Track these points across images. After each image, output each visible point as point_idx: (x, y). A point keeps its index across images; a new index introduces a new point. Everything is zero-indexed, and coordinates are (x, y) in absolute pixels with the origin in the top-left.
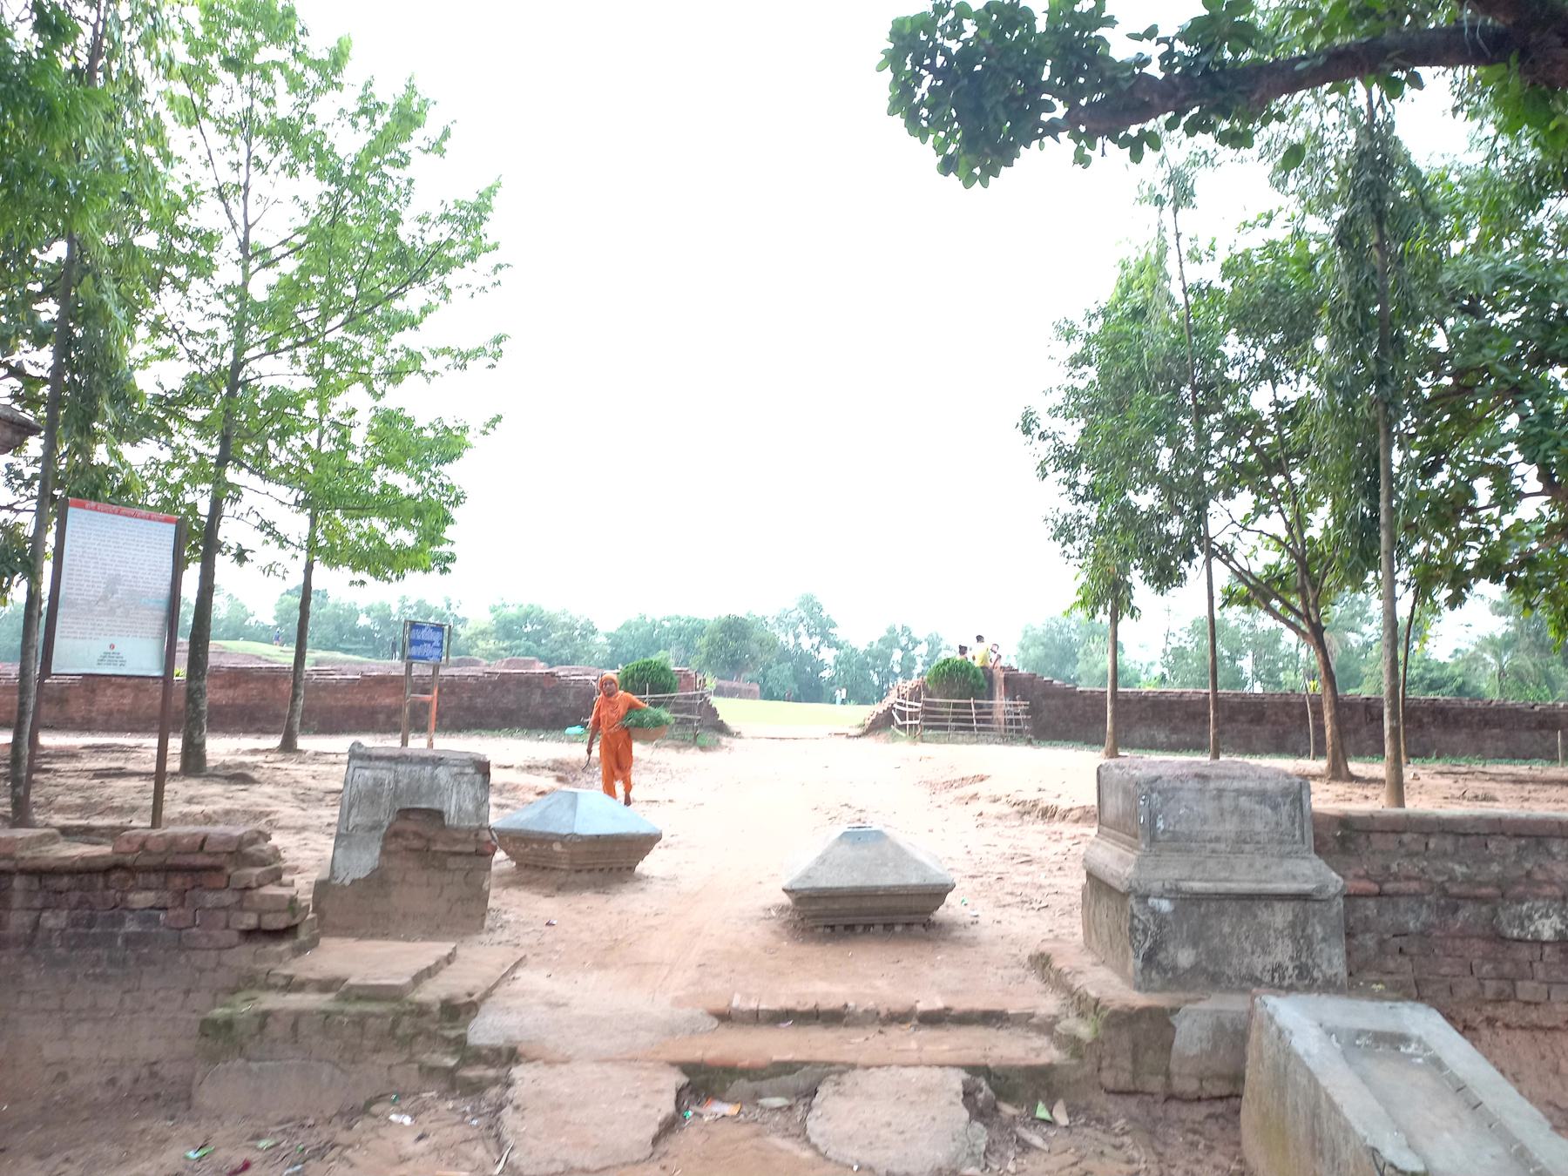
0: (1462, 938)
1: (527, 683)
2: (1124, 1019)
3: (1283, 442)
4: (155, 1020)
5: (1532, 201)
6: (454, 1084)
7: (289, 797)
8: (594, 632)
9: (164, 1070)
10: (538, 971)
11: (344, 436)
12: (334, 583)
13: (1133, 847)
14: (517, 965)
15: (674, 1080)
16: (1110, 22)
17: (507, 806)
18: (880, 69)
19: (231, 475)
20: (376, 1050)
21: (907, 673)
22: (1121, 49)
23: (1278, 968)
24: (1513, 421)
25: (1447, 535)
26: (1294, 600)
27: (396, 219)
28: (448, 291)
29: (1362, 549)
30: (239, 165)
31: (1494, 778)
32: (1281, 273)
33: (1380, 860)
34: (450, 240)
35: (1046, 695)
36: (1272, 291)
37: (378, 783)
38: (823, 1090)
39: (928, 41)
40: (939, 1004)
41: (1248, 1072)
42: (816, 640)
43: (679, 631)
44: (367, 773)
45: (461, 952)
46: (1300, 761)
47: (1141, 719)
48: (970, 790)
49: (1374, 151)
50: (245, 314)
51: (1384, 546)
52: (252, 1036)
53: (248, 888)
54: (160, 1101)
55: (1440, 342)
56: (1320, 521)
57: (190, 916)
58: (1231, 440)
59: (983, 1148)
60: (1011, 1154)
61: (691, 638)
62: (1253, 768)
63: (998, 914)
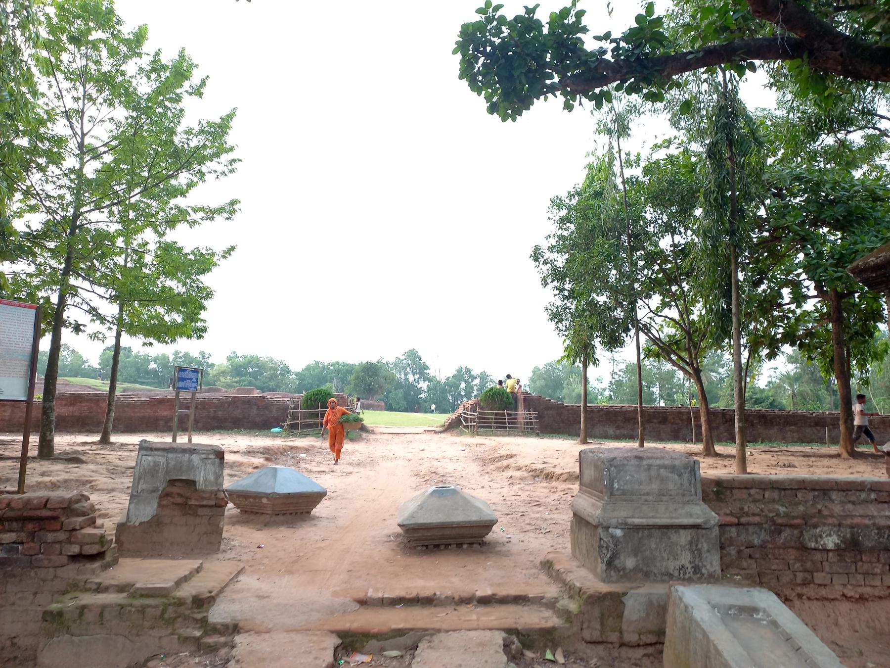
0: (784, 549)
2: (597, 599)
5: (813, 136)
6: (199, 647)
7: (104, 471)
8: (289, 372)
11: (140, 258)
12: (133, 343)
13: (600, 498)
14: (239, 573)
15: (333, 641)
16: (584, 30)
17: (235, 475)
18: (454, 52)
19: (72, 281)
21: (468, 395)
22: (590, 45)
23: (682, 568)
24: (801, 256)
25: (766, 319)
26: (683, 354)
27: (172, 132)
29: (722, 326)
31: (793, 454)
33: (738, 504)
34: (204, 144)
35: (547, 408)
36: (671, 183)
37: (157, 464)
39: (482, 37)
40: (489, 592)
42: (417, 376)
43: (338, 371)
44: (150, 458)
46: (688, 445)
47: (599, 421)
48: (505, 463)
50: (81, 185)
52: (75, 621)
53: (74, 530)
54: (17, 661)
55: (762, 212)
56: (698, 311)
57: (38, 547)
58: (649, 265)
61: (345, 375)
63: (521, 536)
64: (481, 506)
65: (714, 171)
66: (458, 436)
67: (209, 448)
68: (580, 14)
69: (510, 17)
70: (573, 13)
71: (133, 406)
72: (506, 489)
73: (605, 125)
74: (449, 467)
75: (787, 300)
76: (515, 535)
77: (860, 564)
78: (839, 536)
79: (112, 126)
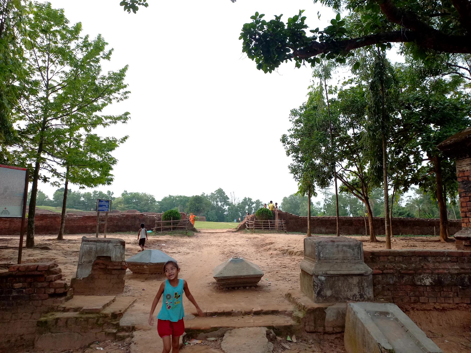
0: (405, 285)
1: (135, 217)
2: (312, 311)
3: (356, 145)
5: (423, 78)
6: (116, 338)
8: (155, 201)
9: (25, 337)
10: (139, 303)
12: (74, 188)
14: (134, 302)
16: (306, 27)
17: (129, 255)
18: (240, 39)
20: (92, 328)
22: (309, 35)
23: (354, 295)
26: (360, 190)
27: (95, 78)
28: (110, 100)
29: (378, 176)
30: (46, 61)
32: (355, 97)
35: (290, 219)
36: (353, 102)
39: (254, 31)
40: (259, 309)
41: (346, 324)
44: (87, 246)
47: (317, 225)
48: (269, 247)
49: (380, 63)
51: (384, 175)
52: (53, 326)
54: (24, 347)
55: (400, 116)
57: (33, 290)
59: (272, 349)
61: (185, 203)
62: (347, 239)
64: (255, 267)
65: (373, 96)
66: (244, 233)
67: (118, 240)
68: (304, 19)
69: (268, 20)
70: (300, 18)
71: (74, 220)
72: (269, 260)
73: (318, 72)
75: (412, 161)
76: (273, 282)
77: (442, 292)
78: (432, 279)
79: (63, 75)
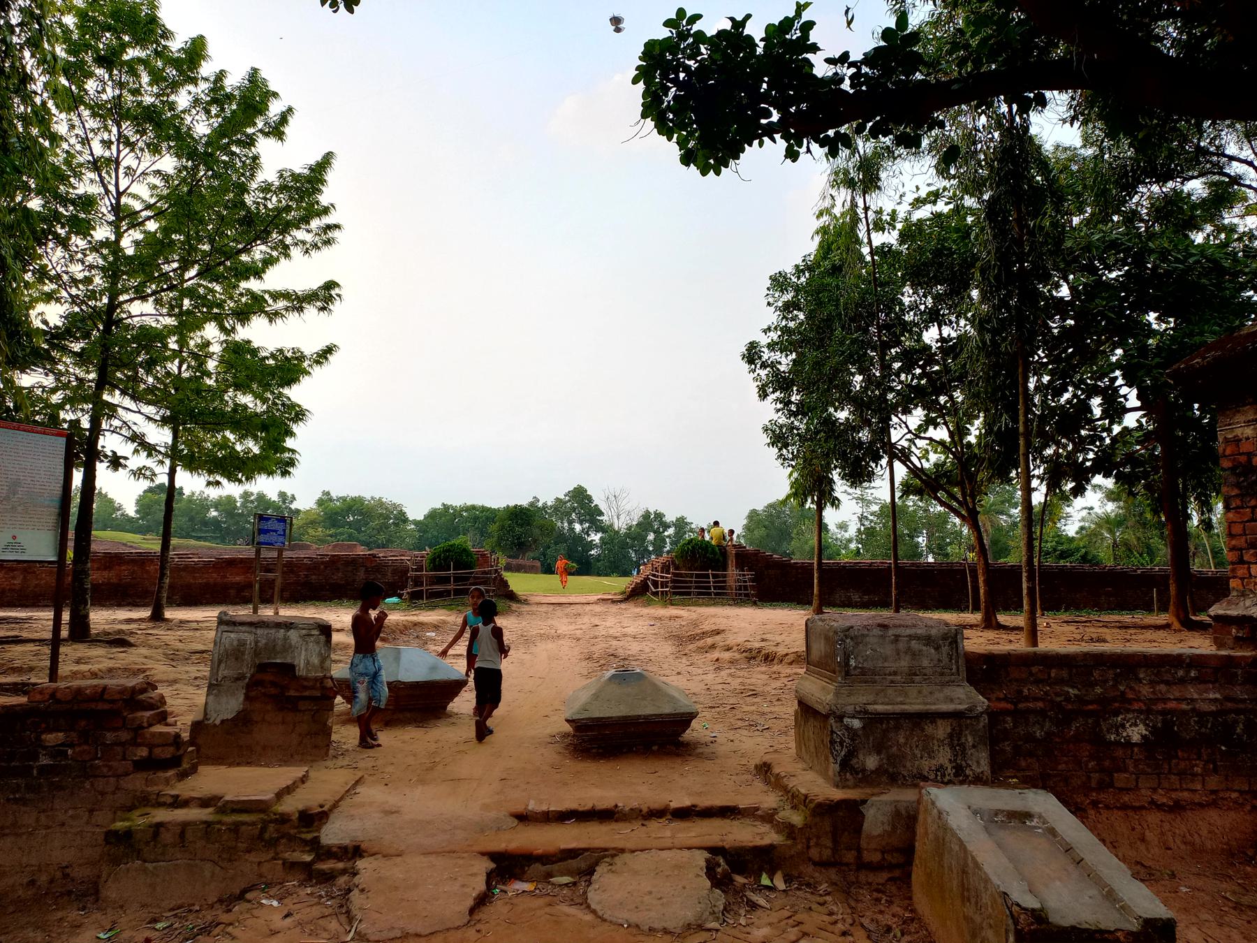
2: (825, 810)
4: (66, 833)
6: (310, 875)
8: (406, 520)
12: (191, 483)
14: (357, 782)
15: (484, 866)
16: (814, 48)
18: (635, 81)
20: (249, 851)
23: (941, 768)
27: (243, 189)
28: (286, 247)
29: (1004, 456)
30: (111, 143)
32: (945, 240)
36: (938, 253)
38: (600, 869)
40: (687, 802)
44: (232, 635)
45: (312, 774)
48: (709, 641)
49: (1012, 147)
50: (116, 266)
52: (147, 843)
55: (1064, 292)
58: (907, 369)
60: (742, 912)
62: (921, 619)
63: (731, 735)
64: (676, 695)
65: (995, 237)
68: (810, 25)
69: (710, 32)
70: (797, 25)
72: (710, 677)
73: (846, 172)
74: (634, 648)
75: (1097, 412)
78: (1146, 725)
79: (157, 181)
